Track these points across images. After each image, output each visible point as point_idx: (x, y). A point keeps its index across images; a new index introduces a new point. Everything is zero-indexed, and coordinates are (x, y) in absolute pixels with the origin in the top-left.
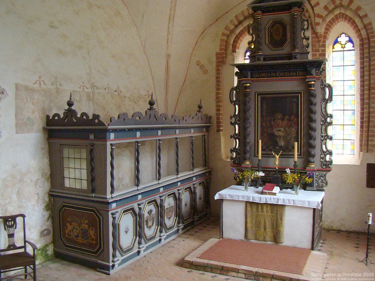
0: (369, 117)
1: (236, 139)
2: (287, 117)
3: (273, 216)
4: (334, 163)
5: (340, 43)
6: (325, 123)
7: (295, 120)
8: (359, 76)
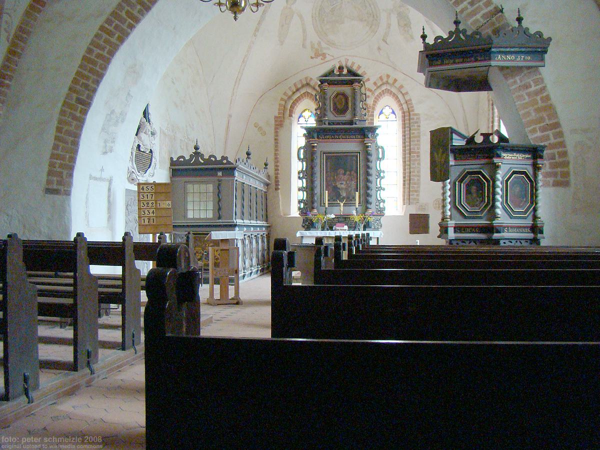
1: (303, 191)
2: (348, 173)
7: (355, 174)
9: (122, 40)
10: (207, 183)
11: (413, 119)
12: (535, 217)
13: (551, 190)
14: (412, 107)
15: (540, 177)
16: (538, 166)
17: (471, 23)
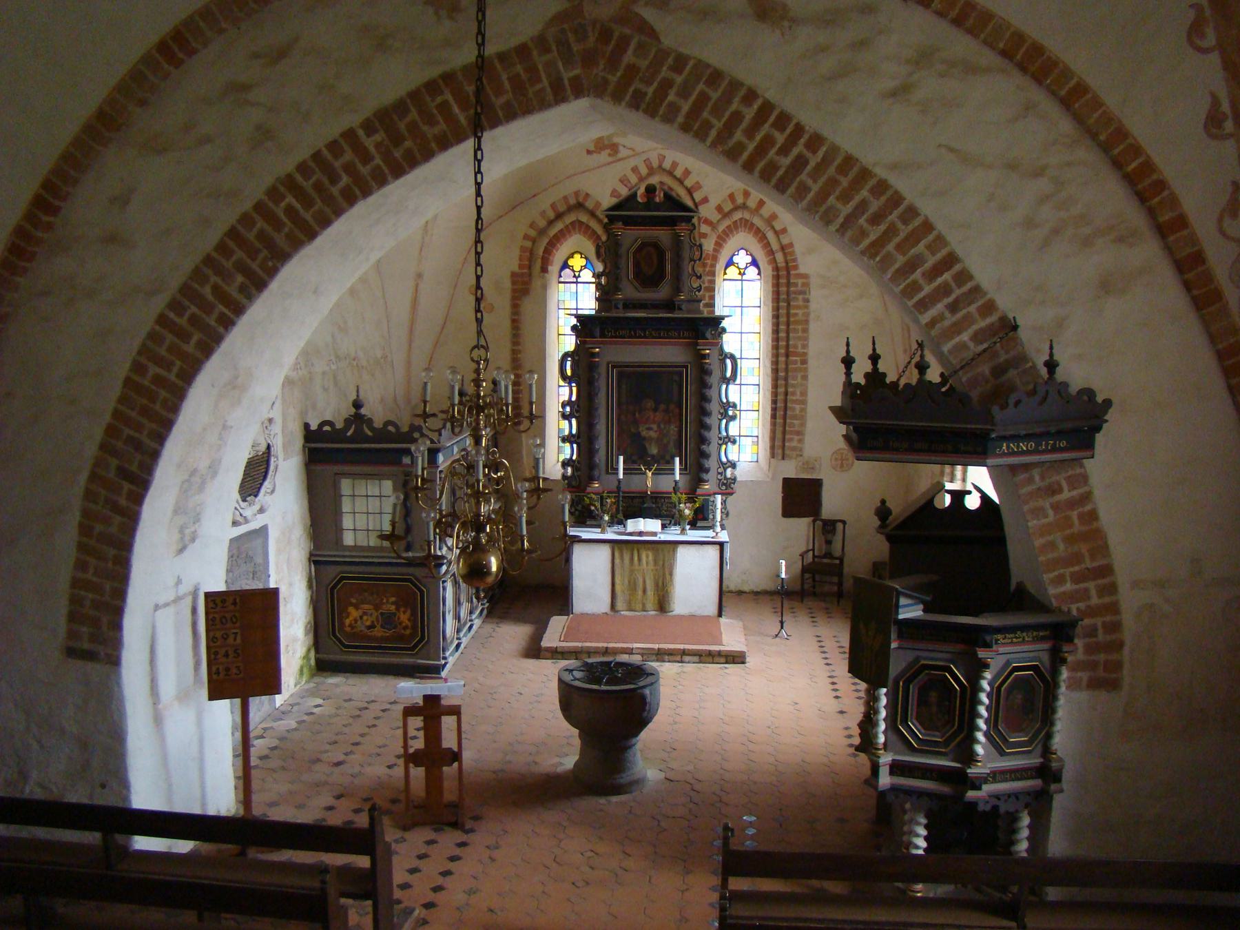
0: (786, 401)
2: (662, 407)
3: (656, 570)
4: (738, 479)
5: (736, 265)
6: (725, 416)
7: (677, 411)
8: (770, 331)
9: (207, 350)
10: (380, 477)
11: (796, 285)
12: (1047, 751)
13: (1083, 696)
14: (795, 260)
15: (1065, 674)
16: (1062, 655)
17: (950, 352)
